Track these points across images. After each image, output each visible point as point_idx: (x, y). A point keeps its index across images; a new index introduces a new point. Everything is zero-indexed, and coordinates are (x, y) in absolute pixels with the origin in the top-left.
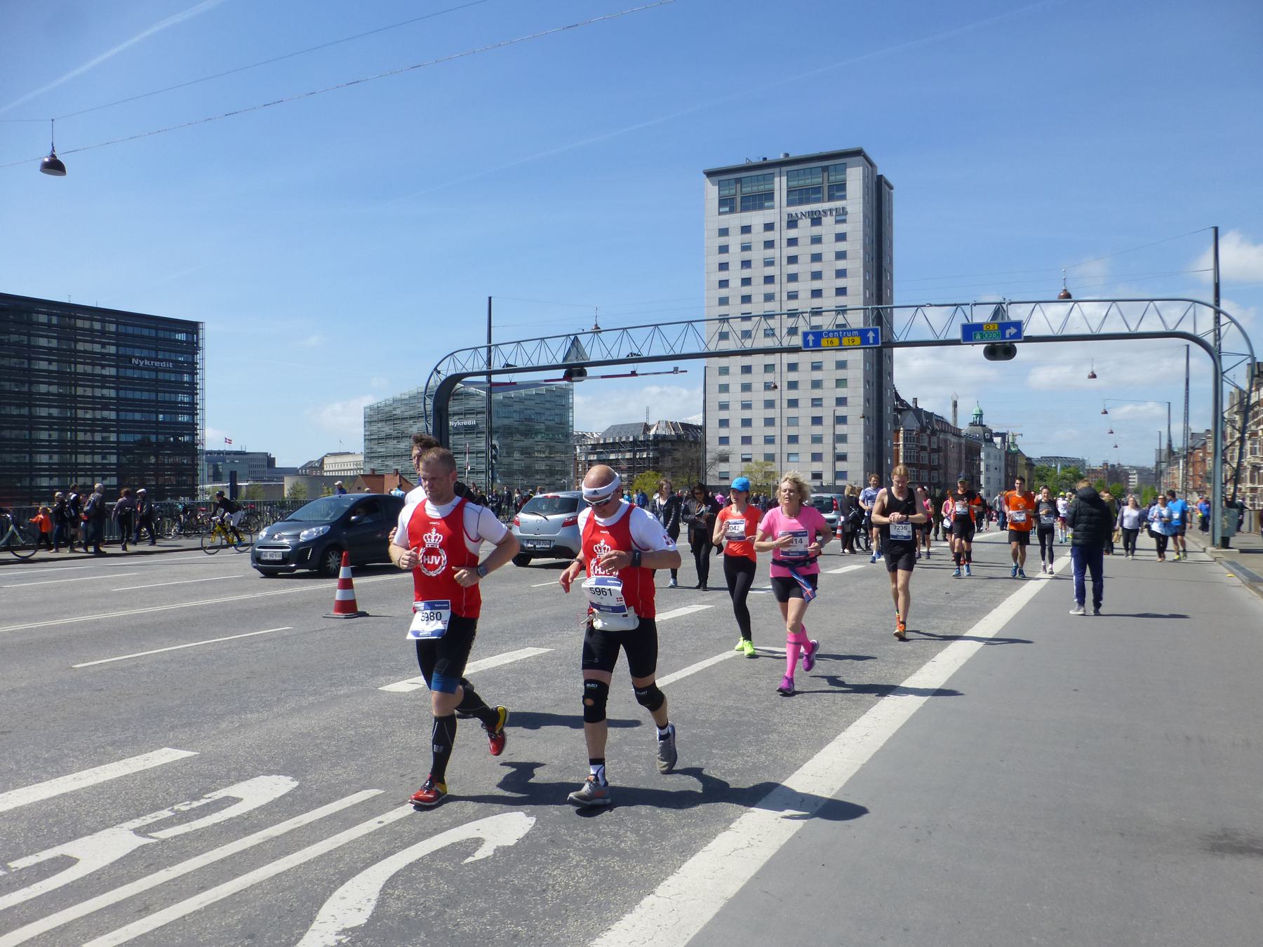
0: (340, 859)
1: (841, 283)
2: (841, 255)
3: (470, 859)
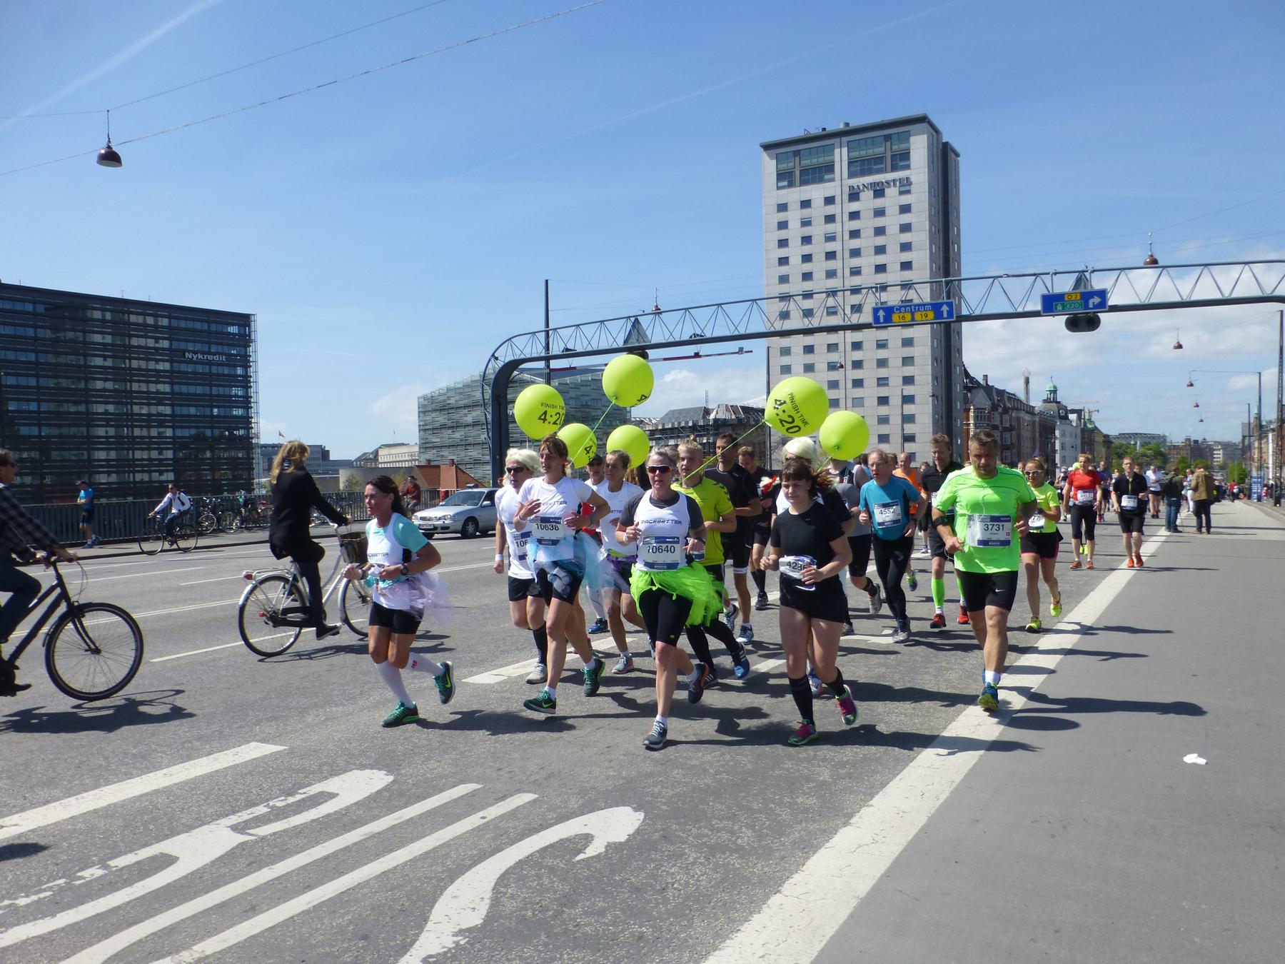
0: (447, 855)
1: (906, 257)
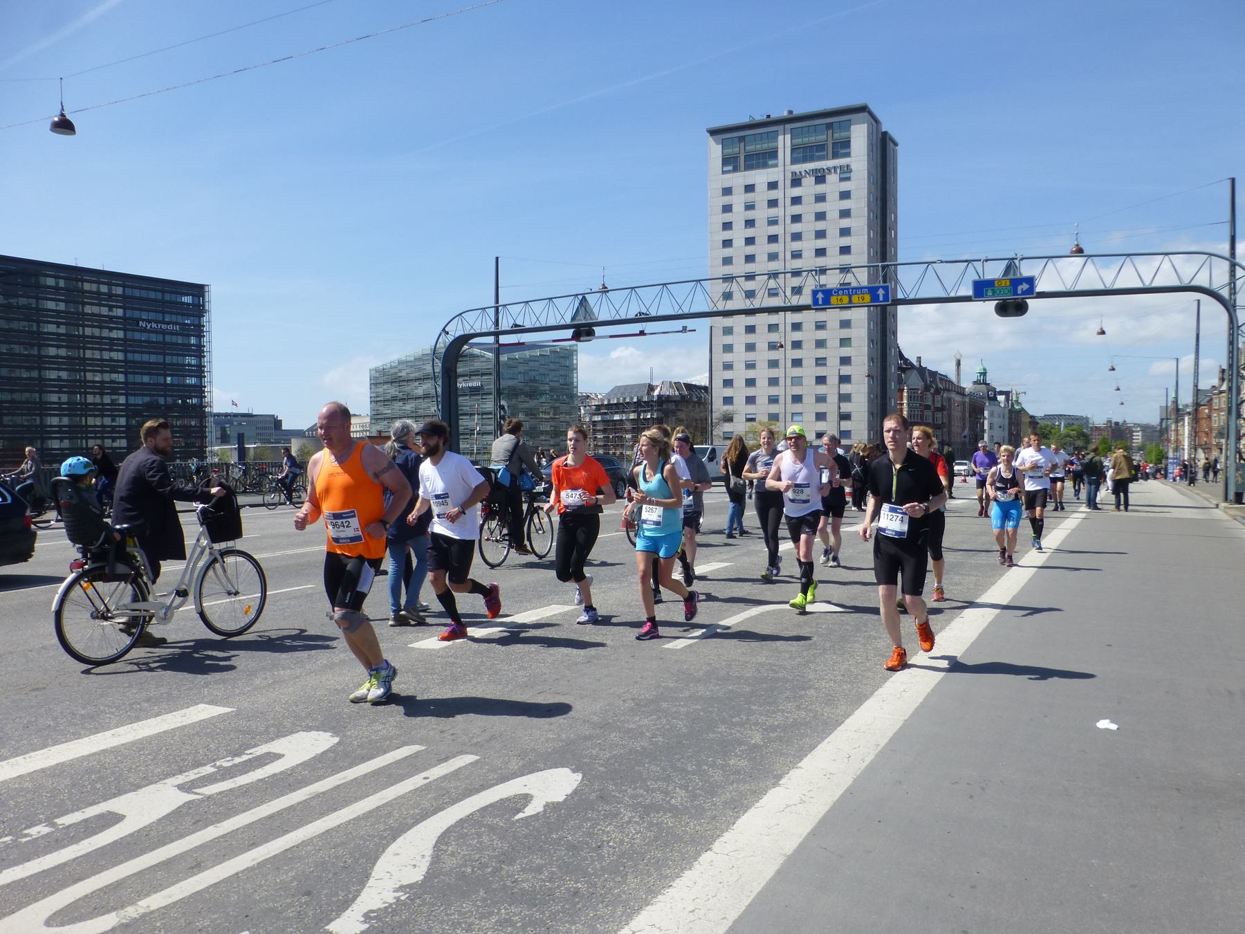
0: (390, 815)
1: (845, 241)
2: (845, 214)
3: (520, 816)
